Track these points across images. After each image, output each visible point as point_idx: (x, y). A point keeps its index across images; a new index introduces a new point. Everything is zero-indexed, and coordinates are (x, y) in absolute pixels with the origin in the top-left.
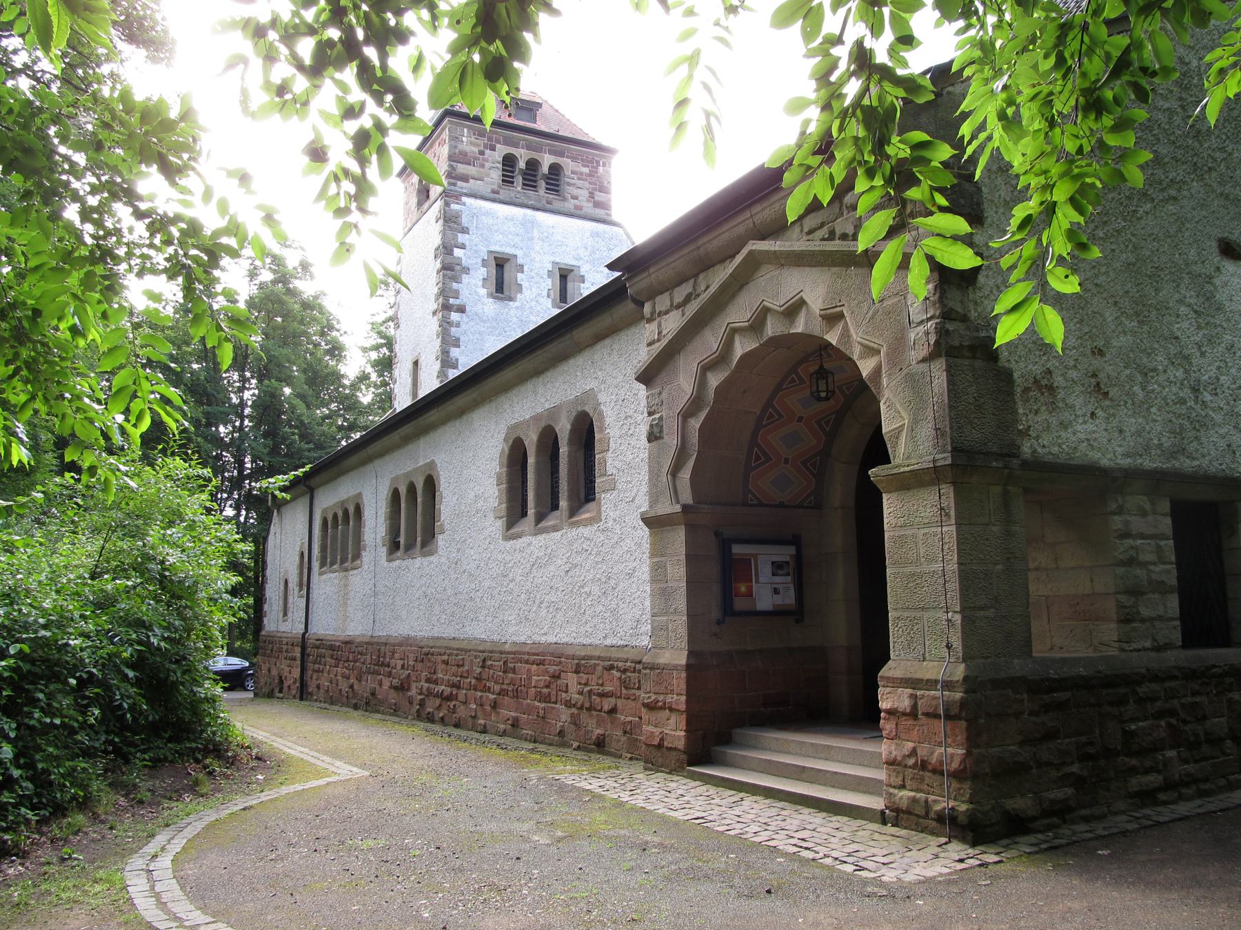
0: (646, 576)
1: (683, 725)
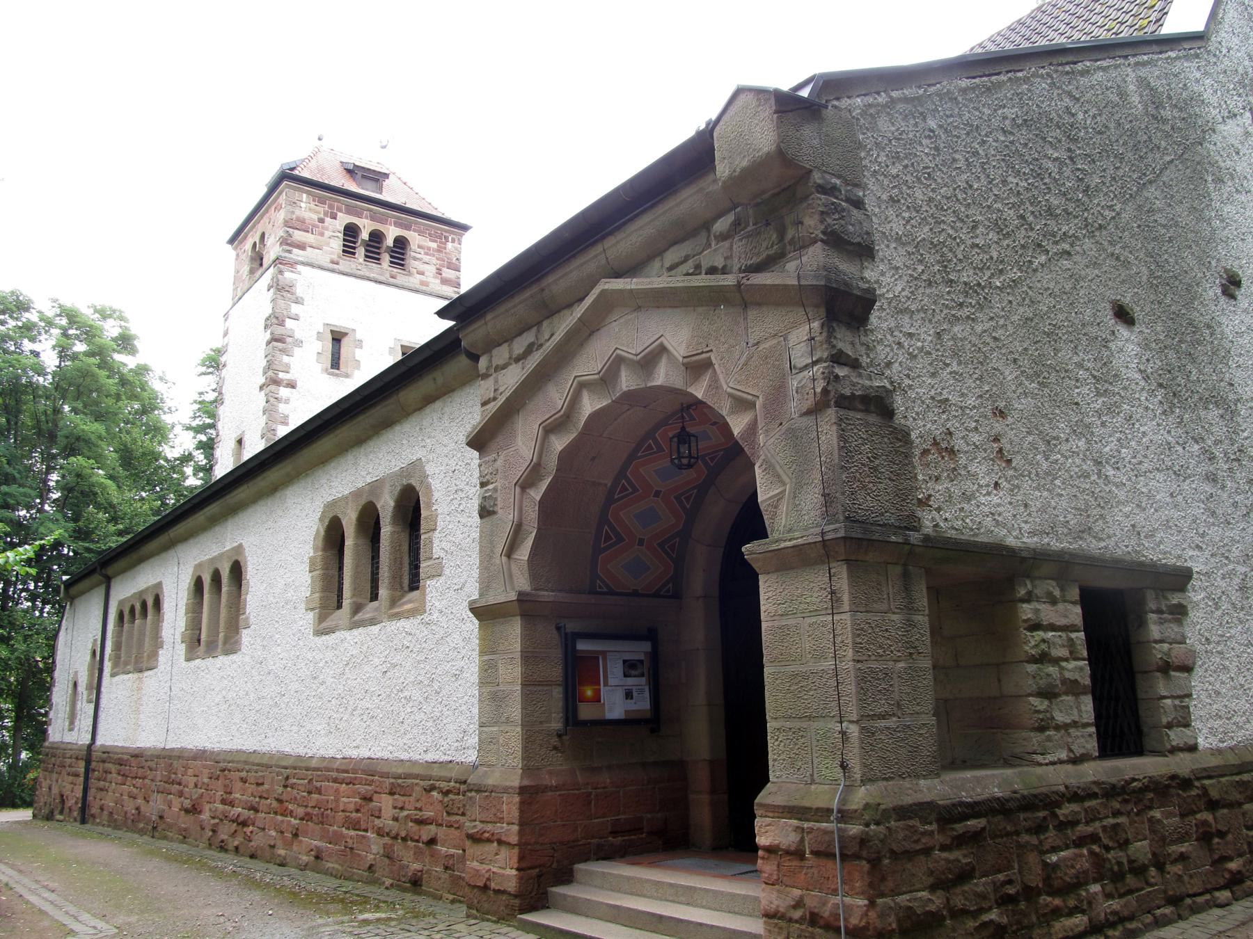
0: (475, 678)
1: (514, 861)
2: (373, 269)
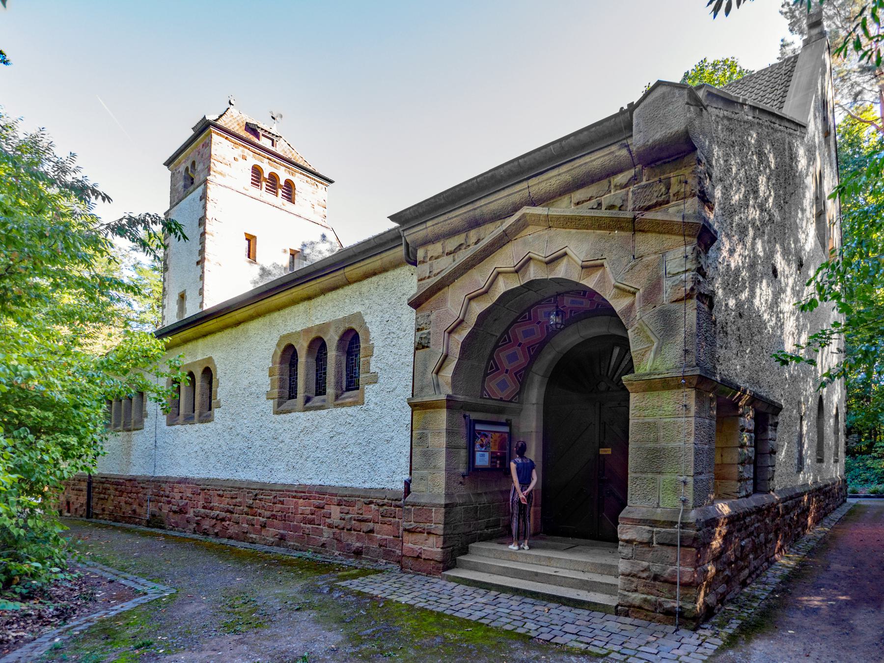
1: (440, 544)
2: (270, 197)
